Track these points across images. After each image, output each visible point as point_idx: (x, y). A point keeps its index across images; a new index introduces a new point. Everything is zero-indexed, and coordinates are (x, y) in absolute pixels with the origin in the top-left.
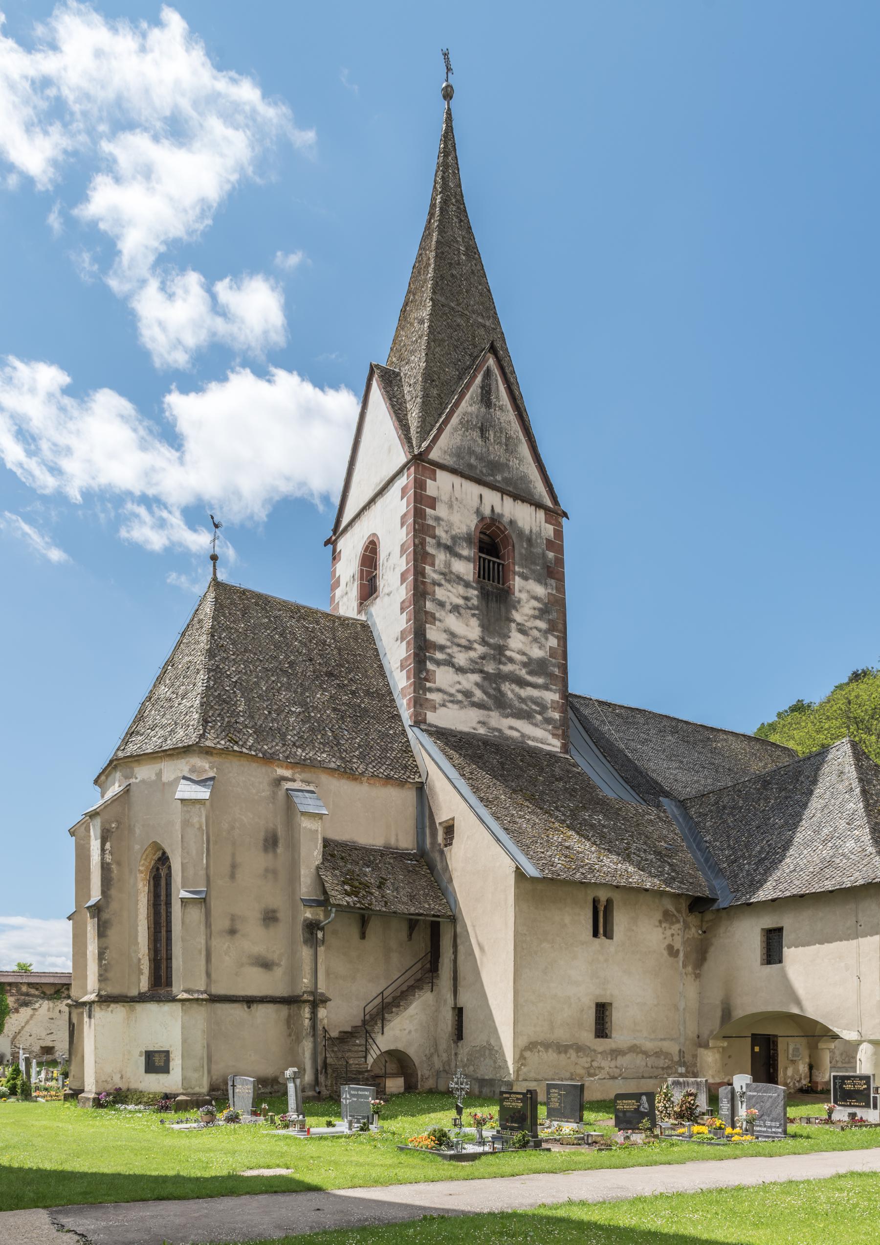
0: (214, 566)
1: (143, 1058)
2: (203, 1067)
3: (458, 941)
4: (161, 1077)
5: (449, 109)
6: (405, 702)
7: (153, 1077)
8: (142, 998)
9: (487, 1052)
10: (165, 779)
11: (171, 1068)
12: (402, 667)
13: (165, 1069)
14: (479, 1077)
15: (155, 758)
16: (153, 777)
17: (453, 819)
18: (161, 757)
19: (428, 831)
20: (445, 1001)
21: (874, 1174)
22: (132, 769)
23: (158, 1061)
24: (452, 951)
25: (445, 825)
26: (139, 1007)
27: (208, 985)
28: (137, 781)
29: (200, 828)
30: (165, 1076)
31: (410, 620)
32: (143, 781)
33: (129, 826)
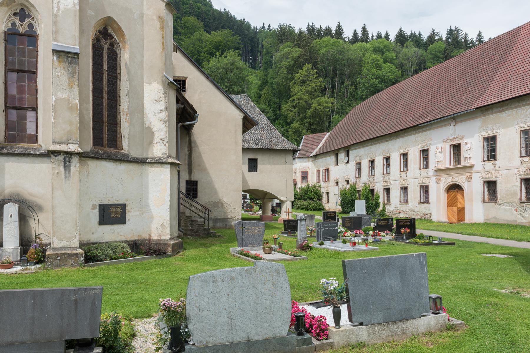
3: (193, 145)
7: (107, 228)
9: (220, 205)
11: (127, 219)
13: (121, 220)
17: (186, 78)
23: (114, 214)
24: (186, 149)
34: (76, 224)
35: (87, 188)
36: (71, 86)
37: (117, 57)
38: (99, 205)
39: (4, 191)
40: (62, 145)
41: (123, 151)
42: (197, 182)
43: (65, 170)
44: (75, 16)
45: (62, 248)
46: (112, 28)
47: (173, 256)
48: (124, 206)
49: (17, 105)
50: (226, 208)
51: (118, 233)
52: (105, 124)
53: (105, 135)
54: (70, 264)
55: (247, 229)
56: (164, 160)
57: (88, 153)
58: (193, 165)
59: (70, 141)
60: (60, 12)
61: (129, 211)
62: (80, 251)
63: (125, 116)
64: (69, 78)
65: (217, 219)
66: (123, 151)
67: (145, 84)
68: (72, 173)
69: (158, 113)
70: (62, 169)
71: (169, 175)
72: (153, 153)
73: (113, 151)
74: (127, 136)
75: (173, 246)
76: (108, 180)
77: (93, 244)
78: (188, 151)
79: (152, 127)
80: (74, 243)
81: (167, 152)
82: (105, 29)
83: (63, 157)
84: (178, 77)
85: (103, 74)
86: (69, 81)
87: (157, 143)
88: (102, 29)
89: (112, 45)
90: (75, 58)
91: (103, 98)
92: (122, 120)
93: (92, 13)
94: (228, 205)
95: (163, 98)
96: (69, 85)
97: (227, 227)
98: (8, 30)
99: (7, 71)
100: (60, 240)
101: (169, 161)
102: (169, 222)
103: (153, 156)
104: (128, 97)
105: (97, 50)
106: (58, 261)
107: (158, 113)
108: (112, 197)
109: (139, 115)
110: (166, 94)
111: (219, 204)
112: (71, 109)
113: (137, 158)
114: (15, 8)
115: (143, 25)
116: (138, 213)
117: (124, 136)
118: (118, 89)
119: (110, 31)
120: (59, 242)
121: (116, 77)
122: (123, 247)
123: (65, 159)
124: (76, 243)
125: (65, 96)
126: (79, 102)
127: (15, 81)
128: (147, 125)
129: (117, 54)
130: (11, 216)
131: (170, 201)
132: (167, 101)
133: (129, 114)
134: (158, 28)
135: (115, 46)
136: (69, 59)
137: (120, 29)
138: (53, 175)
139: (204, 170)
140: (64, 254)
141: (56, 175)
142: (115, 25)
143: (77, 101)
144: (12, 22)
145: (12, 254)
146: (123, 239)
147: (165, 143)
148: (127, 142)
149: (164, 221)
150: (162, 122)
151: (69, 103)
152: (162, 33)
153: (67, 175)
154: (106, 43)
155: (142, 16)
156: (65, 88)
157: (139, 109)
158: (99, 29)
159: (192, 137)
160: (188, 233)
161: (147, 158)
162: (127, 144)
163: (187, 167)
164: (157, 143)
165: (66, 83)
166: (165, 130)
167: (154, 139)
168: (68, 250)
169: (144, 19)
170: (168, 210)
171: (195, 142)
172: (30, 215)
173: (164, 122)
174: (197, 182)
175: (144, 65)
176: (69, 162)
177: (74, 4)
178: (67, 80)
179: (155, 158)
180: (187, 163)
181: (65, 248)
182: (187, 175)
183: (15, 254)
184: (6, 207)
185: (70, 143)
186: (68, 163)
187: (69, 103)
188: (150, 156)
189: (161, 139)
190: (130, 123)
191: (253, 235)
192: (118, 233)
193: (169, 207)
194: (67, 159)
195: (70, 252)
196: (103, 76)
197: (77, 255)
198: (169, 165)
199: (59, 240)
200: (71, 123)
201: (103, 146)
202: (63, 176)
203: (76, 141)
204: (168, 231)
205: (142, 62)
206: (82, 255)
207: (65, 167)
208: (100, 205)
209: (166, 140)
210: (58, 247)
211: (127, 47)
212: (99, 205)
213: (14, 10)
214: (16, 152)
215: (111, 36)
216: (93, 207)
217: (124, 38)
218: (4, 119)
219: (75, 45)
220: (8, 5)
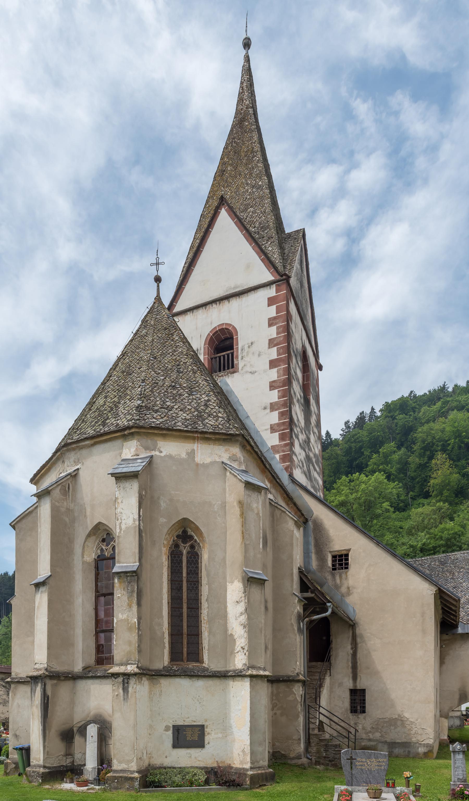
0: (158, 286)
1: (170, 733)
2: (265, 741)
3: (358, 640)
4: (194, 752)
5: (247, 59)
7: (182, 752)
8: (167, 673)
9: (399, 723)
10: (199, 459)
11: (206, 742)
13: (200, 743)
14: (388, 740)
16: (184, 455)
17: (349, 550)
18: (194, 439)
19: (313, 556)
20: (340, 685)
22: (156, 441)
24: (349, 647)
25: (333, 554)
26: (164, 682)
28: (162, 455)
29: (258, 514)
31: (283, 397)
34: (134, 747)
35: (159, 708)
36: (130, 606)
38: (173, 726)
39: (90, 713)
40: (122, 667)
41: (204, 665)
42: (365, 690)
43: (124, 691)
44: (135, 532)
45: (121, 771)
46: (191, 529)
47: (251, 789)
49: (104, 628)
50: (409, 727)
51: (196, 758)
52: (185, 636)
53: (185, 650)
54: (126, 787)
55: (359, 762)
57: (160, 671)
58: (359, 668)
59: (129, 662)
60: (122, 532)
61: (209, 734)
62: (136, 775)
64: (128, 598)
65: (395, 743)
66: (204, 665)
67: (228, 584)
68: (130, 695)
70: (121, 691)
72: (235, 665)
73: (192, 665)
74: (207, 647)
75: (252, 777)
76: (184, 699)
77: (165, 768)
78: (352, 648)
79: (234, 634)
80: (132, 766)
82: (185, 532)
83: (122, 679)
84: (338, 551)
85: (182, 581)
86: (129, 600)
87: (238, 652)
89: (192, 547)
90: (133, 576)
91: (182, 608)
93: (165, 520)
94: (412, 723)
95: (243, 598)
96: (128, 605)
97: (411, 756)
99: (97, 598)
101: (247, 674)
102: (249, 748)
106: (116, 784)
107: (239, 617)
108: (188, 718)
109: (221, 621)
110: (246, 592)
111: (397, 722)
112: (130, 629)
114: (102, 535)
115: (225, 515)
116: (220, 735)
117: (204, 648)
118: (200, 595)
119: (190, 532)
120: (119, 764)
121: (198, 582)
123: (123, 681)
124: (134, 766)
125: (125, 616)
126: (138, 620)
127: (103, 605)
128: (230, 632)
129: (198, 555)
130: (92, 737)
131: (251, 722)
132: (246, 601)
134: (238, 515)
136: (129, 578)
138: (113, 697)
139: (376, 673)
140: (121, 777)
141: (115, 697)
142: (193, 525)
144: (100, 548)
146: (202, 765)
149: (246, 747)
153: (126, 697)
155: (223, 506)
156: (125, 609)
157: (223, 615)
158: (176, 534)
159: (357, 629)
160: (322, 761)
161: (229, 671)
162: (207, 657)
163: (350, 670)
164: (238, 652)
165: (126, 603)
166: (245, 637)
169: (227, 507)
170: (248, 733)
171: (362, 636)
173: (245, 627)
174: (365, 690)
175: (227, 562)
176: (128, 683)
177: (134, 520)
178: (127, 600)
179: (237, 670)
180: (350, 665)
181: (124, 771)
182: (351, 681)
185: (129, 664)
187: (128, 623)
188: (232, 668)
191: (370, 771)
192: (196, 758)
193: (249, 729)
194: (126, 681)
195: (127, 776)
196: (182, 584)
197: (132, 779)
200: (130, 643)
201: (182, 660)
202: (122, 698)
203: (135, 661)
204: (248, 759)
205: (224, 559)
206: (137, 779)
208: (174, 726)
209: (246, 648)
211: (207, 546)
212: (173, 726)
213: (102, 537)
214: (98, 675)
215: (191, 537)
216: (167, 728)
217: (202, 537)
218: (94, 643)
219: (135, 562)
220: (95, 534)
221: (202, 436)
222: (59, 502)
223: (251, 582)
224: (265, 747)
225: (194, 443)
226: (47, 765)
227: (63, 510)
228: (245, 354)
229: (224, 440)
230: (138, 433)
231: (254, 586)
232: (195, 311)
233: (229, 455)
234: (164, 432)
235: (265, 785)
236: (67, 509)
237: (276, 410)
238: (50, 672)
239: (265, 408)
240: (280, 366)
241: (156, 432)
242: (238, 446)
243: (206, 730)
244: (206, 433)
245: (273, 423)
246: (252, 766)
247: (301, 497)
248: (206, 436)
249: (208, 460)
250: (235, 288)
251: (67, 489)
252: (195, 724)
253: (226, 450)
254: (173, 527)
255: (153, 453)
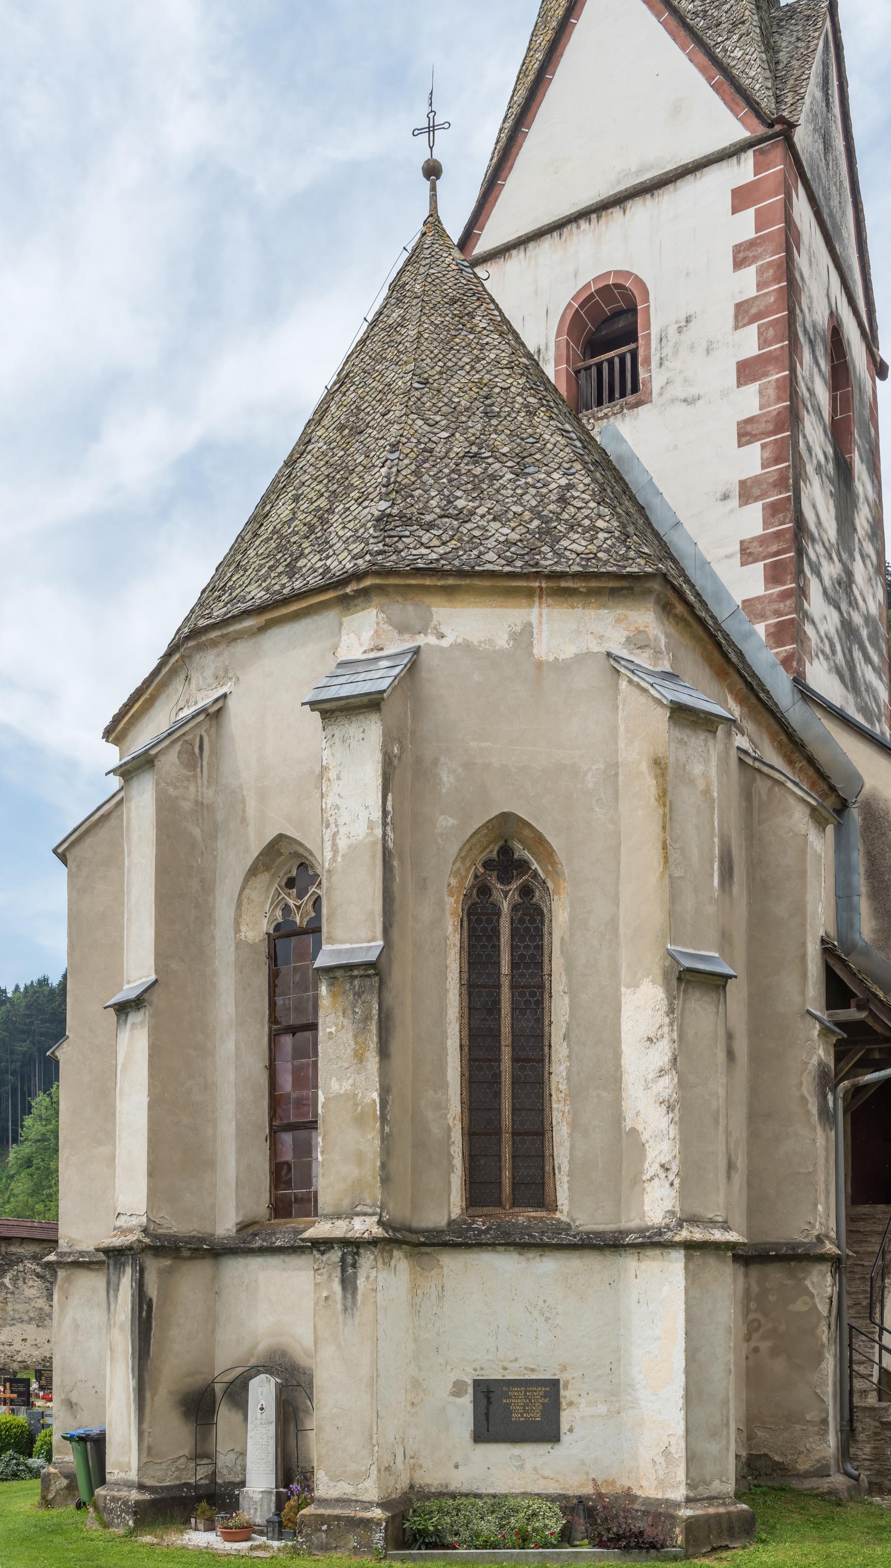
0: (433, 189)
2: (727, 1425)
4: (532, 1454)
6: (760, 629)
7: (500, 1455)
11: (564, 1427)
12: (747, 554)
13: (546, 1431)
15: (510, 593)
16: (502, 641)
18: (530, 594)
21: (3, 1480)
23: (520, 1410)
26: (452, 1264)
27: (757, 1203)
28: (445, 643)
29: (707, 792)
30: (542, 1449)
31: (777, 461)
32: (466, 647)
33: (418, 761)
34: (371, 1438)
35: (438, 1334)
37: (543, 924)
38: (475, 1381)
41: (558, 1215)
43: (344, 1289)
45: (338, 1500)
46: (521, 842)
48: (553, 1387)
49: (292, 1119)
51: (535, 1469)
52: (506, 1137)
54: (351, 1546)
56: (668, 1236)
59: (358, 1209)
61: (571, 1404)
62: (377, 1513)
63: (561, 1106)
64: (355, 1036)
66: (558, 1215)
67: (623, 989)
68: (359, 1297)
69: (654, 1081)
71: (683, 1284)
72: (643, 1216)
73: (524, 1216)
74: (565, 1167)
75: (691, 1525)
76: (503, 1309)
79: (640, 1128)
80: (366, 1490)
81: (677, 1209)
82: (506, 851)
83: (340, 1254)
85: (498, 986)
86: (356, 1043)
87: (652, 1179)
88: (494, 855)
89: (526, 891)
90: (369, 976)
91: (499, 1060)
92: (556, 1116)
93: (451, 821)
95: (666, 1029)
96: (356, 1055)
98: (278, 927)
100: (335, 1478)
101: (677, 1239)
103: (642, 1224)
104: (569, 1046)
105: (479, 921)
106: (324, 1535)
107: (654, 1081)
108: (516, 1360)
109: (604, 1094)
112: (360, 1120)
113: (598, 1234)
116: (602, 1409)
117: (559, 1168)
118: (546, 1023)
119: (521, 851)
120: (332, 1484)
122: (534, 1514)
123: (343, 1260)
125: (347, 1086)
126: (380, 1096)
128: (628, 1124)
129: (542, 914)
130: (262, 1409)
131: (687, 1372)
132: (675, 1036)
133: (573, 1096)
134: (653, 800)
135: (537, 893)
137: (540, 839)
138: (316, 1304)
140: (338, 1518)
141: (322, 1303)
142: (527, 832)
143: (375, 1096)
144: (282, 905)
145: (261, 1505)
146: (553, 1488)
147: (672, 1177)
148: (566, 1186)
149: (673, 1442)
150: (664, 1108)
151: (356, 1105)
152: (661, 812)
153: (349, 1303)
154: (506, 894)
156: (346, 1065)
161: (629, 1232)
164: (652, 1179)
165: (349, 1051)
166: (672, 1136)
167: (646, 1165)
168: (349, 1507)
170: (681, 1402)
172: (307, 1407)
173: (670, 1108)
175: (622, 930)
176: (354, 1266)
178: (353, 1043)
181: (344, 1501)
183: (265, 1507)
184: (254, 1384)
185: (358, 1215)
186: (350, 1271)
189: (662, 1166)
190: (574, 1126)
192: (535, 1469)
194: (349, 1260)
195: (353, 1514)
196: (499, 995)
197: (366, 1523)
198: (682, 1252)
199: (332, 1479)
200: (360, 1158)
202: (339, 1307)
206: (378, 1524)
207: (343, 1281)
208: (477, 1383)
209: (675, 1168)
210: (328, 1496)
211: (566, 886)
212: (475, 1381)
213: (285, 874)
214: (278, 1243)
215: (523, 866)
216: (458, 1389)
217: (554, 864)
218: (268, 1158)
221: (551, 584)
222: (176, 787)
223: (688, 982)
224: (728, 1442)
225: (531, 606)
226: (149, 1482)
227: (187, 806)
228: (668, 350)
229: (613, 593)
230: (381, 589)
231: (697, 994)
232: (531, 245)
233: (626, 633)
234: (451, 581)
235: (727, 1548)
236: (197, 802)
237: (757, 499)
238: (156, 1237)
239: (725, 497)
240: (766, 374)
241: (428, 582)
242: (651, 606)
243: (562, 1393)
244: (563, 575)
245: (747, 536)
246: (692, 1495)
247: (828, 739)
248: (563, 584)
249: (568, 651)
250: (639, 172)
251: (197, 750)
252: (533, 1377)
253: (618, 621)
254: (474, 840)
255: (421, 640)
